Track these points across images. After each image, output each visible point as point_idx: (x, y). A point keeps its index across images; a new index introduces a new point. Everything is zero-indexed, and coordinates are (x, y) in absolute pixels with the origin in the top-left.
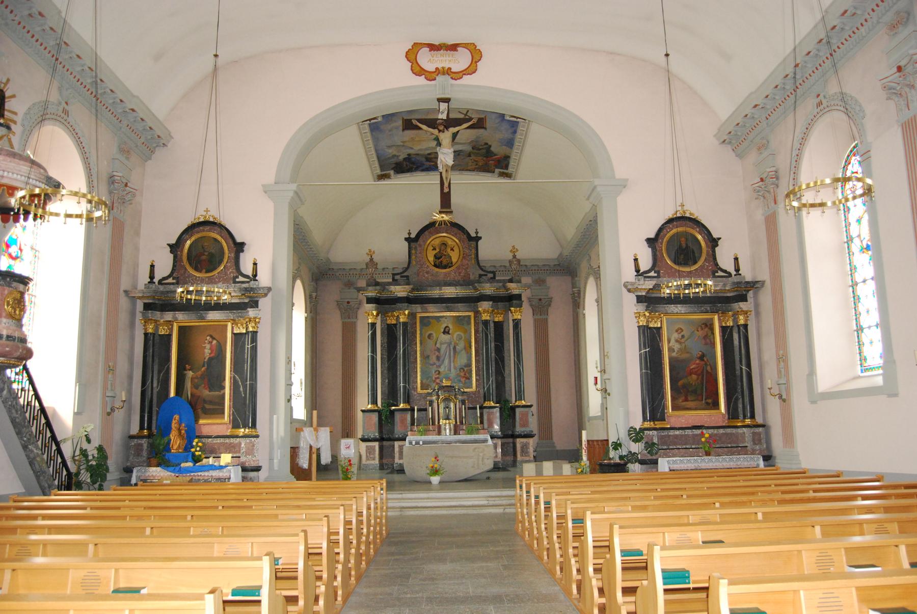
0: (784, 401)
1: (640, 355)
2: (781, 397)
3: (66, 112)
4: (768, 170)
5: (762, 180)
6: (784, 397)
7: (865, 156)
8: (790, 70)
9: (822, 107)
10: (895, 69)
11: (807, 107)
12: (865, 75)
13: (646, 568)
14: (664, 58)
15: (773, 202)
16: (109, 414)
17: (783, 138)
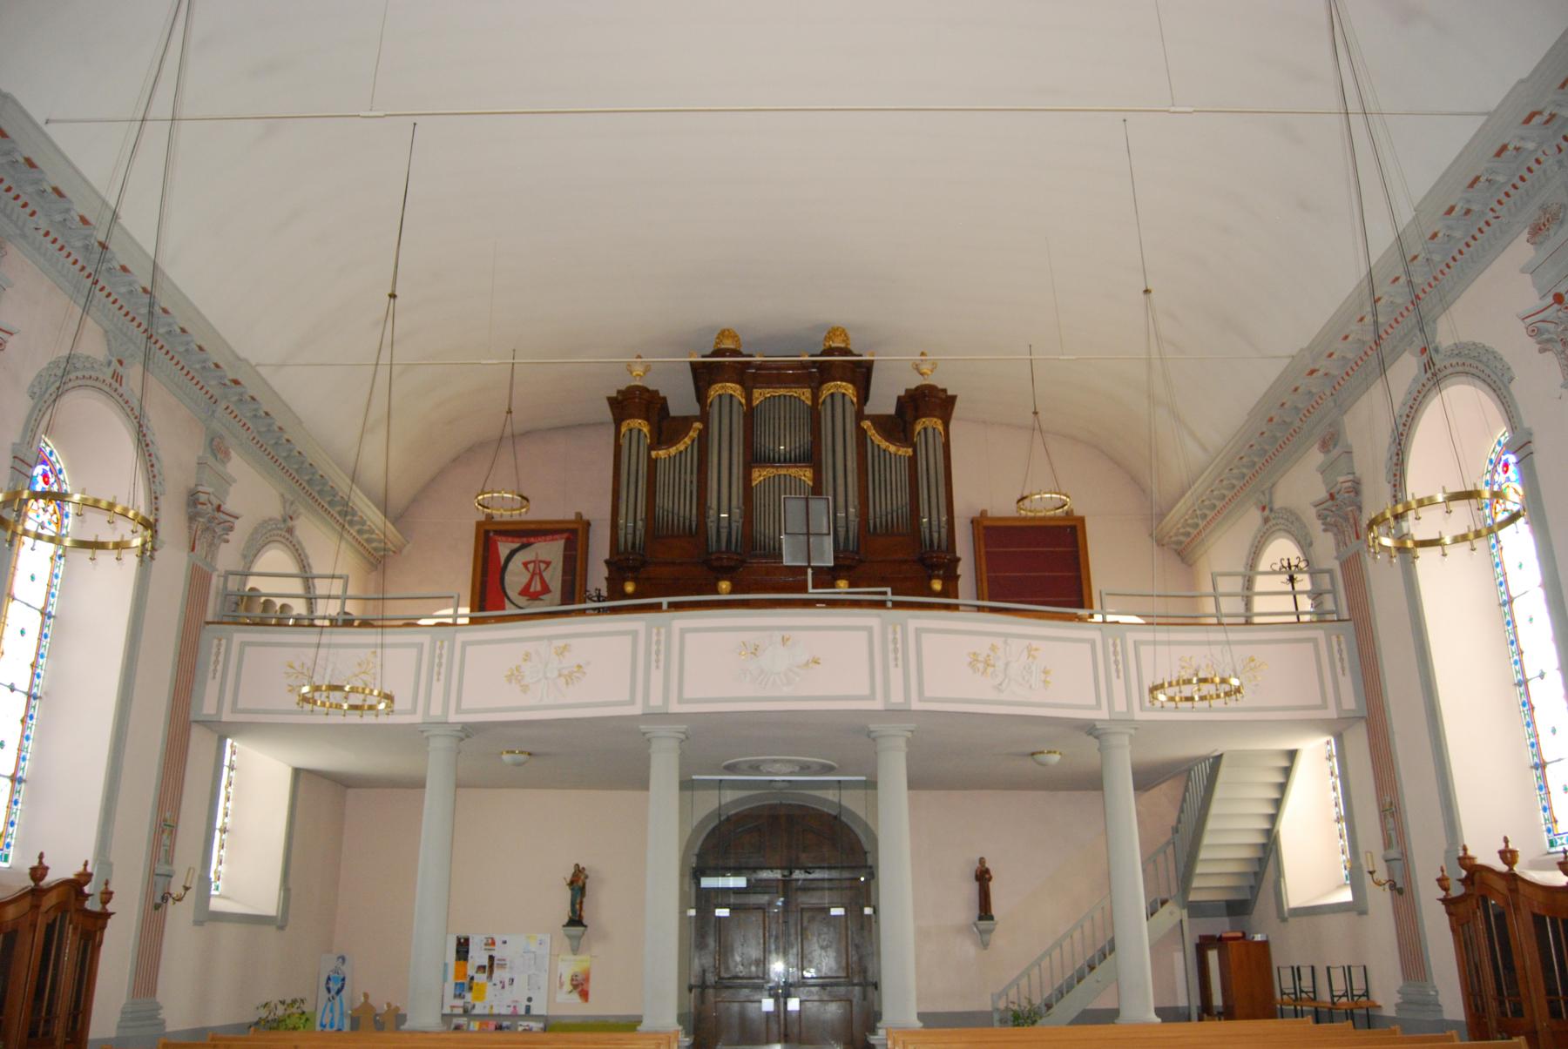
0: (1400, 891)
1: (897, 605)
2: (1393, 886)
3: (117, 377)
4: (1341, 479)
5: (1332, 497)
10: (1550, 300)
11: (1406, 368)
12: (1495, 303)
14: (1142, 295)
15: (1353, 536)
16: (157, 907)
17: (1368, 420)
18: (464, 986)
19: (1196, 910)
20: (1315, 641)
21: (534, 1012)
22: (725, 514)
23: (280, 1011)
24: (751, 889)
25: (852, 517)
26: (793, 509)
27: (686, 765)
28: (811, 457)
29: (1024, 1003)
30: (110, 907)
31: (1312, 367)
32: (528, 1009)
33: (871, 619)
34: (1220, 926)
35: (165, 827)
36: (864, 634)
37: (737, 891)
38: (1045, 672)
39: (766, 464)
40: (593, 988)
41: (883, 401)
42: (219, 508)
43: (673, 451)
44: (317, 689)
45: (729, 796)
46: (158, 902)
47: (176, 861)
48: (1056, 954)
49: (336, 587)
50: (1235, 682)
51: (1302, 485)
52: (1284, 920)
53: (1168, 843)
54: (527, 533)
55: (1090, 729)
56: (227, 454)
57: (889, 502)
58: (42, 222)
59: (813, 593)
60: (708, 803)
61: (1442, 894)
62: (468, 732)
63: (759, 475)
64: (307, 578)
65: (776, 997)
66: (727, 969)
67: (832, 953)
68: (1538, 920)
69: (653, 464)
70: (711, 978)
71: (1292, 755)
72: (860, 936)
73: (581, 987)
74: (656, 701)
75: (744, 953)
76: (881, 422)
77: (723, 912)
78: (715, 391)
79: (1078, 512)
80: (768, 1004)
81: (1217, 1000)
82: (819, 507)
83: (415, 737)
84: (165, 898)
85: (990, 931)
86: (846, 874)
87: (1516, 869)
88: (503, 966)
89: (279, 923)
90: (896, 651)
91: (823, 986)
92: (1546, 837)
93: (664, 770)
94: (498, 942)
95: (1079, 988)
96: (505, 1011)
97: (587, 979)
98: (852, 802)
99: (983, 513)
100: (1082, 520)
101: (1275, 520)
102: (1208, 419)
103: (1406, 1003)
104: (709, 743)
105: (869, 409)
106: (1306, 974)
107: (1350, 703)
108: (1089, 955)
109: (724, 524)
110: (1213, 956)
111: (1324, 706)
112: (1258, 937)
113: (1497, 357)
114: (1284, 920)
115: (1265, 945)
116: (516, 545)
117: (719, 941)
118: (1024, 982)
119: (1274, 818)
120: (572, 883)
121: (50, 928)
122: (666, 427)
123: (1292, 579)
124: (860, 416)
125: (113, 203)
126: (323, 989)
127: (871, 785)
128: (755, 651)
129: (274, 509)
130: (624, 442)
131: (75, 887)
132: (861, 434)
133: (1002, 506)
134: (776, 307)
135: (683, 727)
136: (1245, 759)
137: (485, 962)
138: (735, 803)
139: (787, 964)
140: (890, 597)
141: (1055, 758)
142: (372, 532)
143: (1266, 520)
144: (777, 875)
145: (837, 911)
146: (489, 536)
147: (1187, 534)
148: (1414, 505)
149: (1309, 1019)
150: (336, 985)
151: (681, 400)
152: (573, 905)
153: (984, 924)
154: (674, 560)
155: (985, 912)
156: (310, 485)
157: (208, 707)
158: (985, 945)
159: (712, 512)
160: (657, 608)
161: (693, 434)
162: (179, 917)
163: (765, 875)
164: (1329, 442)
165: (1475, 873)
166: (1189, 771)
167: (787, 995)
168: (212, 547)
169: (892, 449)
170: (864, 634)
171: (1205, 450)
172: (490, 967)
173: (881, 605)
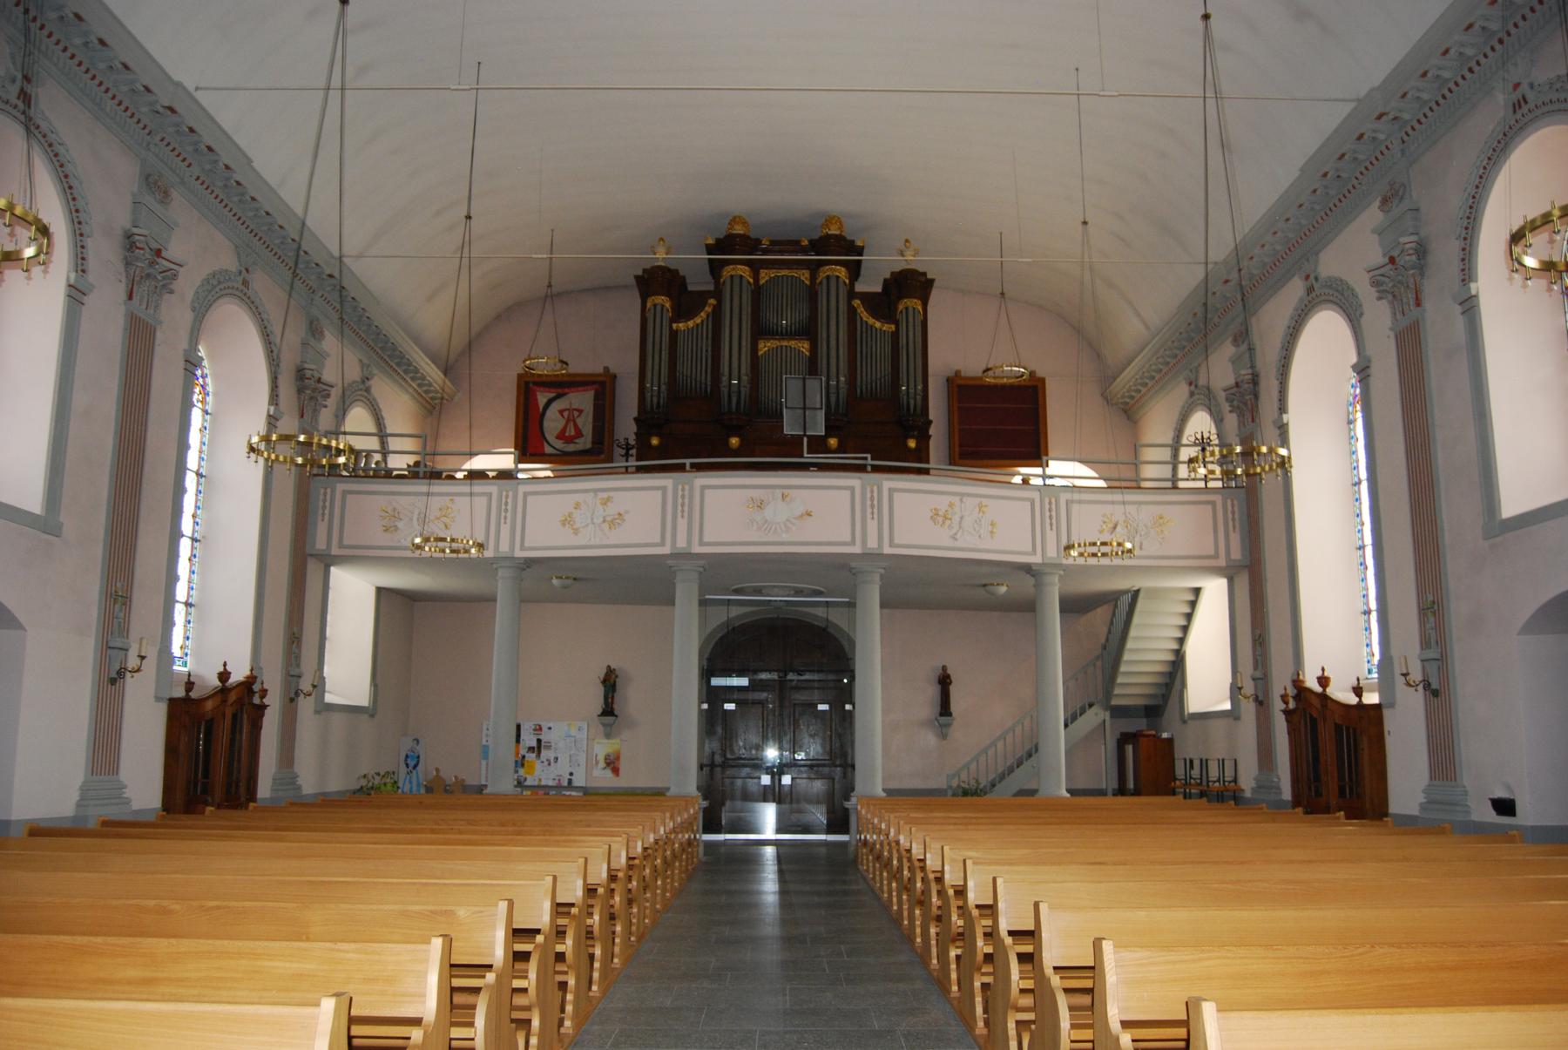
0: (1435, 693)
1: (876, 469)
6: (1434, 686)
7: (1467, 305)
8: (1199, 310)
9: (1525, 109)
10: (1386, 260)
13: (522, 601)
14: (1080, 227)
16: (113, 681)
17: (1273, 315)
18: (521, 762)
19: (1118, 712)
20: (1213, 503)
21: (575, 784)
22: (735, 380)
23: (377, 781)
24: (754, 686)
25: (842, 385)
26: (792, 387)
27: (703, 590)
28: (808, 331)
29: (973, 782)
30: (266, 701)
31: (1381, 110)
32: (570, 781)
33: (853, 481)
34: (1139, 724)
35: (294, 639)
36: (848, 493)
37: (740, 689)
38: (992, 524)
39: (770, 335)
40: (623, 765)
41: (870, 284)
42: (319, 381)
43: (691, 324)
44: (427, 540)
45: (735, 611)
46: (292, 698)
47: (303, 664)
48: (1000, 745)
49: (408, 444)
50: (1128, 545)
51: (1221, 370)
52: (1184, 722)
53: (1097, 658)
54: (562, 385)
55: (1027, 569)
56: (322, 333)
57: (874, 372)
58: (196, 171)
59: (808, 457)
60: (719, 617)
61: (1283, 706)
62: (529, 563)
63: (764, 347)
64: (382, 435)
65: (773, 775)
66: (732, 752)
67: (818, 740)
68: (1338, 728)
69: (674, 335)
70: (718, 759)
71: (1197, 591)
72: (840, 729)
73: (613, 764)
74: (681, 543)
75: (746, 737)
76: (867, 298)
77: (730, 706)
78: (727, 271)
79: (1040, 374)
80: (766, 780)
81: (1131, 785)
82: (814, 385)
83: (487, 567)
84: (297, 694)
85: (949, 725)
86: (831, 677)
87: (1329, 691)
88: (548, 747)
89: (369, 712)
90: (872, 506)
91: (811, 767)
92: (1366, 666)
93: (686, 594)
94: (545, 729)
95: (1018, 772)
96: (551, 783)
97: (618, 758)
98: (837, 618)
99: (958, 373)
100: (1043, 381)
101: (1200, 396)
102: (1144, 309)
103: (1260, 787)
104: (720, 573)
105: (860, 287)
106: (1197, 764)
107: (1237, 554)
108: (1027, 748)
109: (734, 389)
110: (1129, 749)
111: (1216, 556)
112: (1165, 735)
113: (1355, 296)
114: (1184, 722)
115: (1170, 741)
116: (552, 395)
117: (725, 729)
118: (973, 766)
119: (1181, 641)
120: (604, 682)
121: (234, 716)
122: (686, 303)
123: (1203, 450)
124: (852, 294)
125: (336, 254)
126: (403, 765)
127: (852, 605)
128: (761, 505)
129: (227, 261)
130: (650, 316)
131: (248, 684)
132: (852, 311)
133: (972, 366)
134: (779, 196)
135: (702, 562)
136: (1155, 593)
137: (534, 744)
138: (738, 617)
139: (781, 749)
140: (870, 461)
141: (1003, 589)
142: (430, 385)
143: (1192, 394)
144: (775, 676)
145: (822, 707)
146: (528, 386)
147: (1132, 397)
148: (738, 793)
149: (1181, 797)
150: (413, 762)
151: (699, 281)
152: (606, 698)
153: (944, 720)
154: (693, 424)
155: (945, 708)
156: (384, 352)
157: (320, 544)
158: (944, 736)
159: (725, 379)
160: (680, 468)
161: (708, 309)
162: (306, 706)
163: (764, 676)
164: (1243, 336)
165: (1301, 690)
166: (1116, 600)
167: (781, 773)
168: (315, 412)
169: (878, 325)
170: (848, 493)
171: (1147, 326)
172: (538, 748)
173: (860, 469)
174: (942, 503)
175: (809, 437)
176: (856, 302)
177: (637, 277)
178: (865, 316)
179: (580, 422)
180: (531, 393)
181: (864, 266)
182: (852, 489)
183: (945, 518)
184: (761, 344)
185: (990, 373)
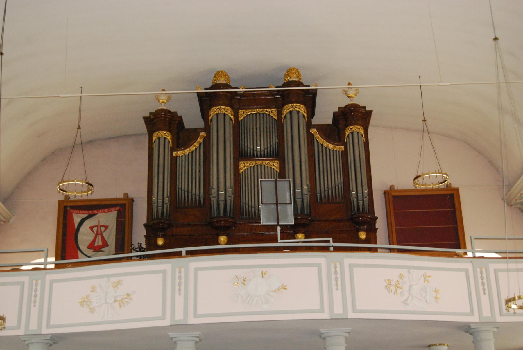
14: (493, 43)
22: (222, 190)
25: (305, 192)
28: (278, 153)
38: (436, 291)
41: (324, 115)
43: (187, 151)
54: (92, 208)
55: (467, 328)
57: (330, 181)
59: (281, 243)
63: (243, 166)
69: (174, 160)
74: (179, 317)
82: (284, 186)
90: (336, 279)
99: (392, 187)
100: (457, 190)
105: (315, 121)
116: (85, 216)
122: (182, 136)
124: (309, 125)
128: (244, 282)
130: (155, 146)
132: (310, 138)
133: (404, 183)
135: (197, 333)
140: (332, 244)
146: (66, 209)
151: (192, 118)
159: (214, 191)
160: (179, 255)
161: (200, 140)
169: (331, 146)
170: (315, 269)
173: (326, 249)
174: (393, 275)
175: (281, 226)
176: (313, 131)
177: (145, 118)
178: (321, 140)
179: (105, 235)
180: (69, 215)
181: (318, 92)
182: (319, 266)
183: (397, 287)
184: (241, 112)
185: (420, 179)
